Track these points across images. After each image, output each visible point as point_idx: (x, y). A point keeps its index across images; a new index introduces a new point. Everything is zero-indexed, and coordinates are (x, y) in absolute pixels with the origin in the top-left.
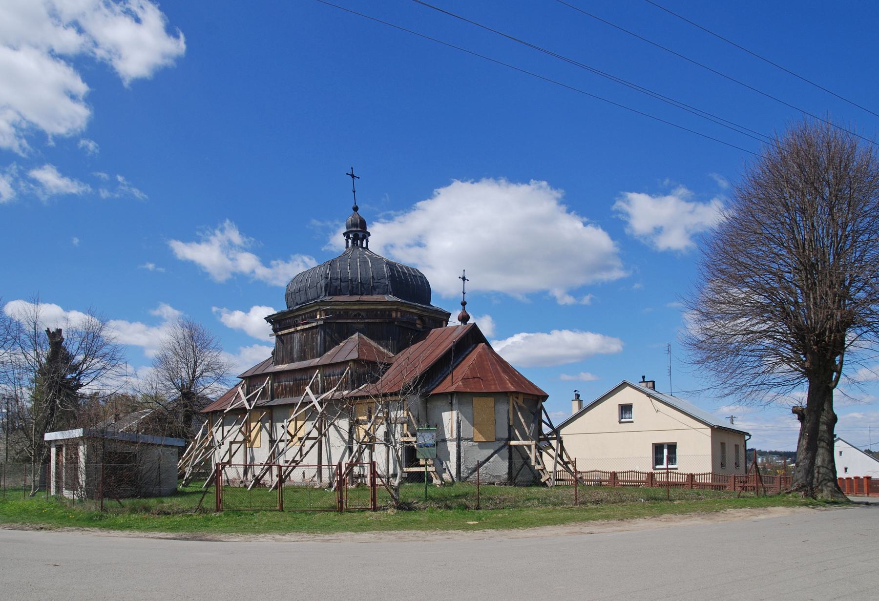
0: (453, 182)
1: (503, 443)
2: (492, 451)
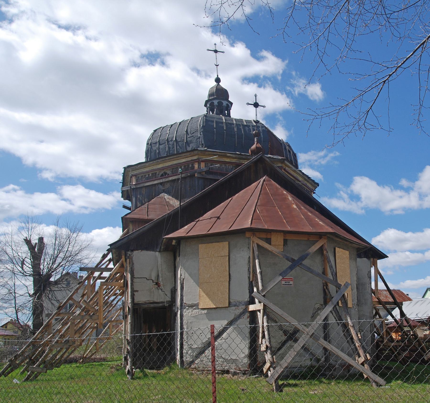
0: (316, 83)
1: (241, 309)
2: (225, 323)
